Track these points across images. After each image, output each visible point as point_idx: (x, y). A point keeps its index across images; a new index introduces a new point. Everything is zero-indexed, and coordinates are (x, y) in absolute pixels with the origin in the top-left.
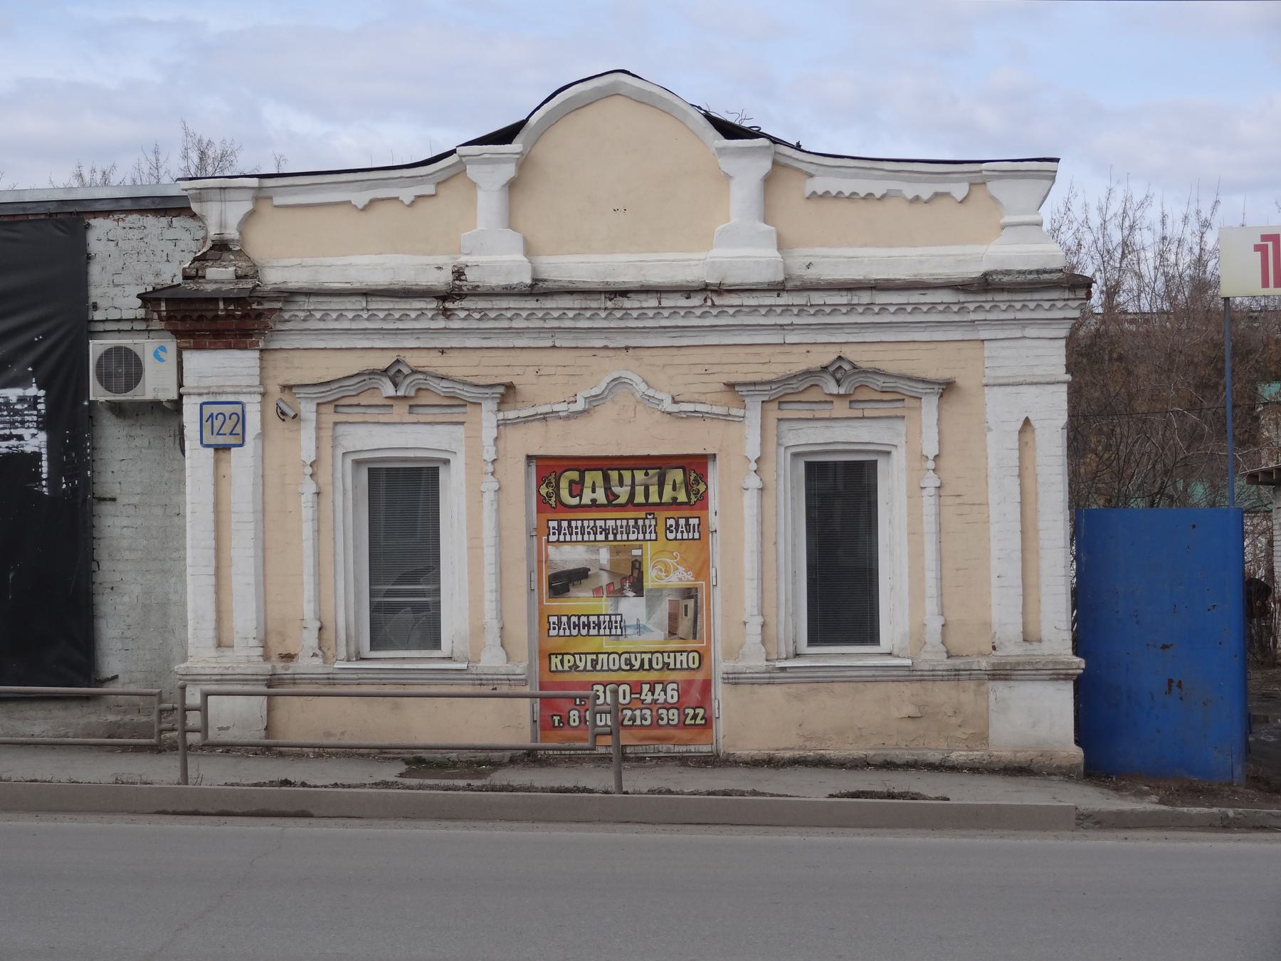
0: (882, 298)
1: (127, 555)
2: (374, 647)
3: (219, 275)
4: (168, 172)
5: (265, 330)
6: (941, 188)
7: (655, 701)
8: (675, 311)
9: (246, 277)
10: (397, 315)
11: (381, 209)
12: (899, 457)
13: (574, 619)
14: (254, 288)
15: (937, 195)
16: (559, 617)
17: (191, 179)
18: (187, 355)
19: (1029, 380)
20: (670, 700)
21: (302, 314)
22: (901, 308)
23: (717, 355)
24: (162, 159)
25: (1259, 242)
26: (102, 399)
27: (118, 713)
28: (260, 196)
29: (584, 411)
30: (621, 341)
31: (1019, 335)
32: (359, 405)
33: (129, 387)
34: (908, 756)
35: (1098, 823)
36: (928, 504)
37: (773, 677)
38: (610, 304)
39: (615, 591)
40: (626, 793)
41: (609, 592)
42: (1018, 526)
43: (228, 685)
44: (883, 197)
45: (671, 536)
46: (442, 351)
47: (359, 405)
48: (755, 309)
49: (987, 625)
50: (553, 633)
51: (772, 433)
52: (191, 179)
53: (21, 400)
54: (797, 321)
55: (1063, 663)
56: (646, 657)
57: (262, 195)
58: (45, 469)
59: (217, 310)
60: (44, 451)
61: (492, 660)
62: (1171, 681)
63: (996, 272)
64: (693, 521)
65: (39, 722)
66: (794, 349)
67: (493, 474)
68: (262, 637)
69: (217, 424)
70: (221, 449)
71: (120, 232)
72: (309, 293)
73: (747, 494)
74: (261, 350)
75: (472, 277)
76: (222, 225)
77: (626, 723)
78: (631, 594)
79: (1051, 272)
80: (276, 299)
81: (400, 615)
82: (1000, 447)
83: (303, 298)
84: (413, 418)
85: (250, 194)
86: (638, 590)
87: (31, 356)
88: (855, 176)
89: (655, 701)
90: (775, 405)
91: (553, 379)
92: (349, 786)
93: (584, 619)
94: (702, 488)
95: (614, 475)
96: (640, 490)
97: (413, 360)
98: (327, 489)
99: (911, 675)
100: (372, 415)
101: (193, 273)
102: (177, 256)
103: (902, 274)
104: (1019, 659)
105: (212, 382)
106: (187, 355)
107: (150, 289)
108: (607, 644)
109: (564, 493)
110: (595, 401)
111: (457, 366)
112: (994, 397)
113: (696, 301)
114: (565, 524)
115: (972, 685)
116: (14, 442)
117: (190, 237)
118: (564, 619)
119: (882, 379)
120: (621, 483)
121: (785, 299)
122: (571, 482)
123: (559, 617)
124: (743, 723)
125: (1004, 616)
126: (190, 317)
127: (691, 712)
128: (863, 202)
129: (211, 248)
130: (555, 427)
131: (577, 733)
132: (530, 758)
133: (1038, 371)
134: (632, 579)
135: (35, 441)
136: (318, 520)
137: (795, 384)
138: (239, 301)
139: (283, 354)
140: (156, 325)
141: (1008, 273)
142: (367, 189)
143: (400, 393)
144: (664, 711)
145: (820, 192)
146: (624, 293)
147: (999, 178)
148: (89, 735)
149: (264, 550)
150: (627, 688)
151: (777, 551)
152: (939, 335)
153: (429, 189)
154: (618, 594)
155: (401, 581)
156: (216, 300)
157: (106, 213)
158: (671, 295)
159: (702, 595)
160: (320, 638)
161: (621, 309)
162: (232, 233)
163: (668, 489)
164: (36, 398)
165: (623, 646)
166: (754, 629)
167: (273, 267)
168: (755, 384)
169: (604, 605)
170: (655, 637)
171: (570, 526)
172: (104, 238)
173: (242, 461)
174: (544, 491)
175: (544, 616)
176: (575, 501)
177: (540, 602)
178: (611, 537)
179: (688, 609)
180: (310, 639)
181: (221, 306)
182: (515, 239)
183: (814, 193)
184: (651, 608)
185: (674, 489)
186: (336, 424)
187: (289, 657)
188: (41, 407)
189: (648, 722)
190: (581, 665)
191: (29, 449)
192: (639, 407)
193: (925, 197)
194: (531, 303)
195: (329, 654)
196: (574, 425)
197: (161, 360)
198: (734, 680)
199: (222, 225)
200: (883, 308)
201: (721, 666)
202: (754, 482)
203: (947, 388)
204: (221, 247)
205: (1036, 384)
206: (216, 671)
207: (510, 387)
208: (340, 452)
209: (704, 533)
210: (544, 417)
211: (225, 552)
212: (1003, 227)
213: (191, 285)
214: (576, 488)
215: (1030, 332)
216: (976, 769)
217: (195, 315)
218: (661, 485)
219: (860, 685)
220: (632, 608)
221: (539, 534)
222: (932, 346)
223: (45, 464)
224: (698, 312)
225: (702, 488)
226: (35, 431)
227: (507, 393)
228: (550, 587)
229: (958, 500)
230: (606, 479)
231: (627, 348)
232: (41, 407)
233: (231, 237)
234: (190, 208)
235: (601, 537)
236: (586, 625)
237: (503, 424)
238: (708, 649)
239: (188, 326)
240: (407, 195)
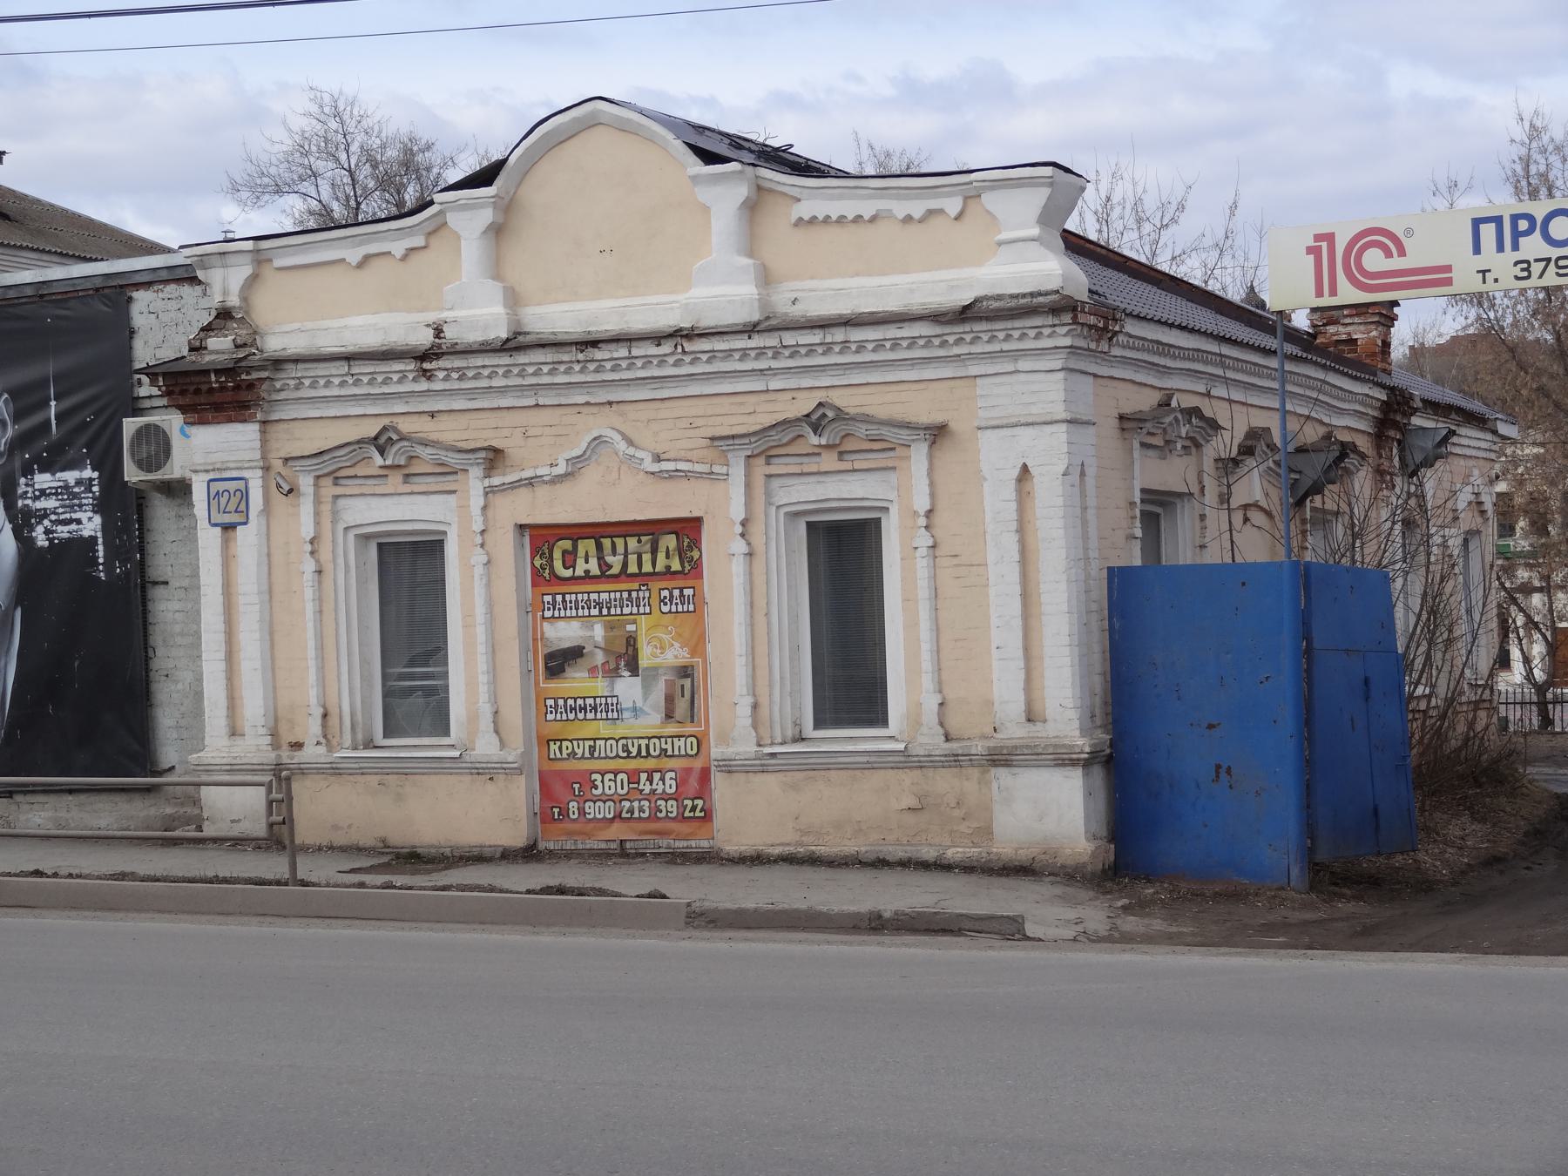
0: (857, 335)
1: (179, 640)
2: (387, 733)
5: (257, 402)
6: (934, 204)
7: (653, 792)
8: (648, 361)
9: (244, 345)
10: (380, 379)
11: (377, 264)
12: (894, 510)
13: (570, 702)
15: (931, 213)
16: (556, 700)
19: (1023, 420)
20: (668, 791)
21: (292, 383)
22: (879, 346)
23: (699, 407)
25: (1312, 243)
26: (134, 480)
27: (176, 805)
29: (567, 475)
30: (603, 396)
31: (1010, 368)
32: (356, 477)
33: (158, 468)
34: (901, 853)
35: (712, 921)
36: (922, 565)
37: (764, 765)
38: (581, 356)
39: (610, 671)
40: (304, 883)
41: (604, 672)
42: (1018, 589)
43: (236, 774)
44: (873, 219)
45: (665, 609)
46: (432, 415)
47: (356, 477)
48: (729, 353)
49: (989, 703)
50: (550, 717)
51: (759, 491)
53: (79, 482)
54: (775, 364)
55: (1064, 746)
56: (643, 742)
58: (101, 554)
60: (99, 534)
61: (486, 747)
62: (1218, 767)
63: (987, 298)
64: (688, 592)
65: (105, 814)
66: (779, 396)
67: (482, 545)
68: (272, 723)
69: (223, 501)
70: (228, 528)
71: (160, 304)
72: (297, 360)
73: (735, 559)
75: (450, 333)
76: (225, 292)
77: (624, 815)
78: (627, 673)
79: (1047, 294)
80: (262, 368)
81: (411, 700)
82: (998, 500)
84: (408, 488)
85: (248, 258)
86: (634, 669)
87: (84, 439)
88: (841, 198)
89: (653, 792)
90: (761, 460)
91: (540, 442)
92: (79, 876)
93: (580, 702)
94: (696, 554)
95: (607, 542)
96: (633, 558)
97: (405, 426)
98: (328, 568)
99: (906, 761)
100: (370, 486)
101: (197, 344)
103: (892, 305)
104: (1018, 742)
105: (217, 458)
108: (604, 729)
109: (558, 564)
110: (577, 465)
111: (448, 431)
112: (988, 440)
113: (666, 348)
114: (559, 598)
115: (975, 773)
116: (74, 527)
118: (561, 702)
119: (864, 426)
120: (614, 553)
121: (757, 341)
122: (564, 553)
123: (556, 700)
124: (747, 814)
125: (1006, 691)
127: (689, 803)
128: (853, 226)
130: (542, 491)
131: (576, 826)
132: (530, 854)
133: (1034, 410)
134: (627, 658)
135: (91, 525)
136: (320, 600)
137: (776, 437)
139: (282, 426)
141: (999, 297)
142: (360, 244)
143: (389, 462)
144: (662, 803)
145: (806, 218)
146: (594, 344)
147: (992, 188)
148: (148, 828)
149: (271, 634)
150: (624, 776)
151: (769, 624)
152: (929, 373)
153: (419, 241)
154: (612, 673)
155: (411, 663)
156: (206, 372)
157: (147, 285)
158: (641, 344)
159: (699, 674)
160: (324, 726)
161: (593, 361)
162: (234, 301)
163: (661, 556)
164: (91, 480)
165: (620, 731)
166: (744, 710)
168: (733, 437)
169: (600, 686)
170: (652, 721)
171: (564, 600)
172: (145, 310)
173: (247, 537)
174: (538, 563)
175: (541, 699)
176: (568, 573)
177: (537, 683)
178: (605, 611)
179: (685, 690)
180: (315, 727)
181: (213, 378)
182: (494, 290)
183: (801, 219)
184: (647, 689)
185: (668, 557)
186: (336, 497)
187: (297, 746)
188: (95, 489)
189: (646, 815)
190: (579, 752)
191: (86, 533)
192: (624, 468)
193: (917, 215)
194: (505, 360)
195: (334, 742)
196: (562, 489)
198: (728, 768)
199: (225, 292)
200: (861, 347)
201: (716, 751)
202: (740, 546)
203: (937, 433)
204: (224, 314)
205: (1032, 424)
206: (224, 761)
207: (497, 452)
208: (341, 526)
209: (698, 601)
210: (530, 482)
211: (254, 634)
212: (1000, 244)
214: (569, 558)
215: (1024, 365)
216: (968, 868)
217: (192, 388)
218: (654, 552)
219: (858, 773)
220: (628, 689)
221: (535, 611)
222: (922, 386)
223: (101, 548)
224: (671, 360)
225: (696, 554)
226: (90, 514)
227: (494, 458)
228: (547, 668)
229: (955, 561)
230: (599, 547)
231: (610, 403)
232: (95, 489)
235: (595, 612)
236: (582, 708)
237: (489, 492)
238: (706, 733)
239: (187, 400)
240: (398, 248)
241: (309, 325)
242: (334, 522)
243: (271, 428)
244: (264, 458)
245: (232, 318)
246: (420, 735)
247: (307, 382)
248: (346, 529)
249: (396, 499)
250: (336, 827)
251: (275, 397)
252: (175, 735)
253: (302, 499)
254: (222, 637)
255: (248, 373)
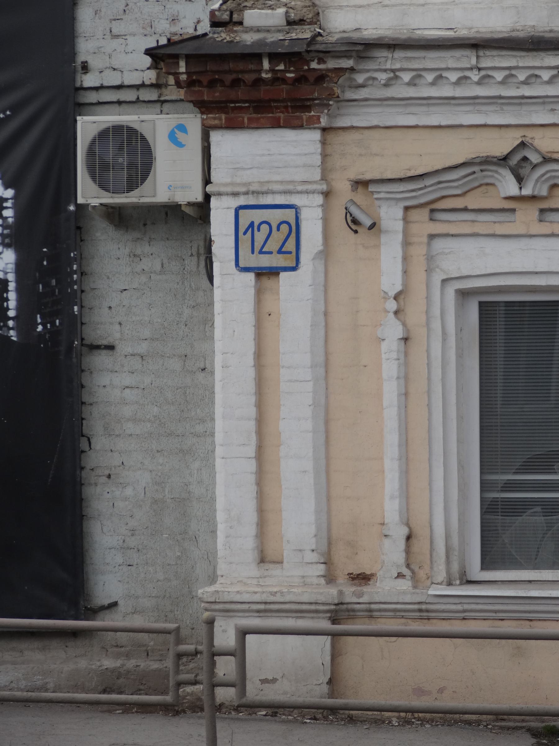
1: (130, 428)
2: (486, 565)
5: (329, 99)
9: (301, 22)
21: (383, 77)
26: (95, 202)
27: (117, 656)
32: (465, 210)
43: (274, 617)
47: (465, 210)
58: (12, 303)
60: (11, 277)
69: (260, 237)
70: (265, 274)
80: (346, 55)
84: (545, 228)
101: (226, 17)
136: (405, 378)
148: (77, 688)
149: (327, 422)
155: (526, 468)
156: (257, 57)
160: (408, 551)
173: (295, 291)
180: (393, 553)
181: (266, 65)
186: (432, 237)
187: (363, 578)
195: (422, 574)
206: (257, 598)
217: (228, 78)
223: (12, 296)
239: (218, 94)
242: (429, 271)
243: (335, 139)
244: (324, 178)
246: (536, 567)
247: (406, 77)
248: (444, 281)
249: (524, 242)
250: (419, 691)
251: (350, 95)
252: (119, 559)
253: (384, 238)
254: (252, 425)
255: (321, 61)
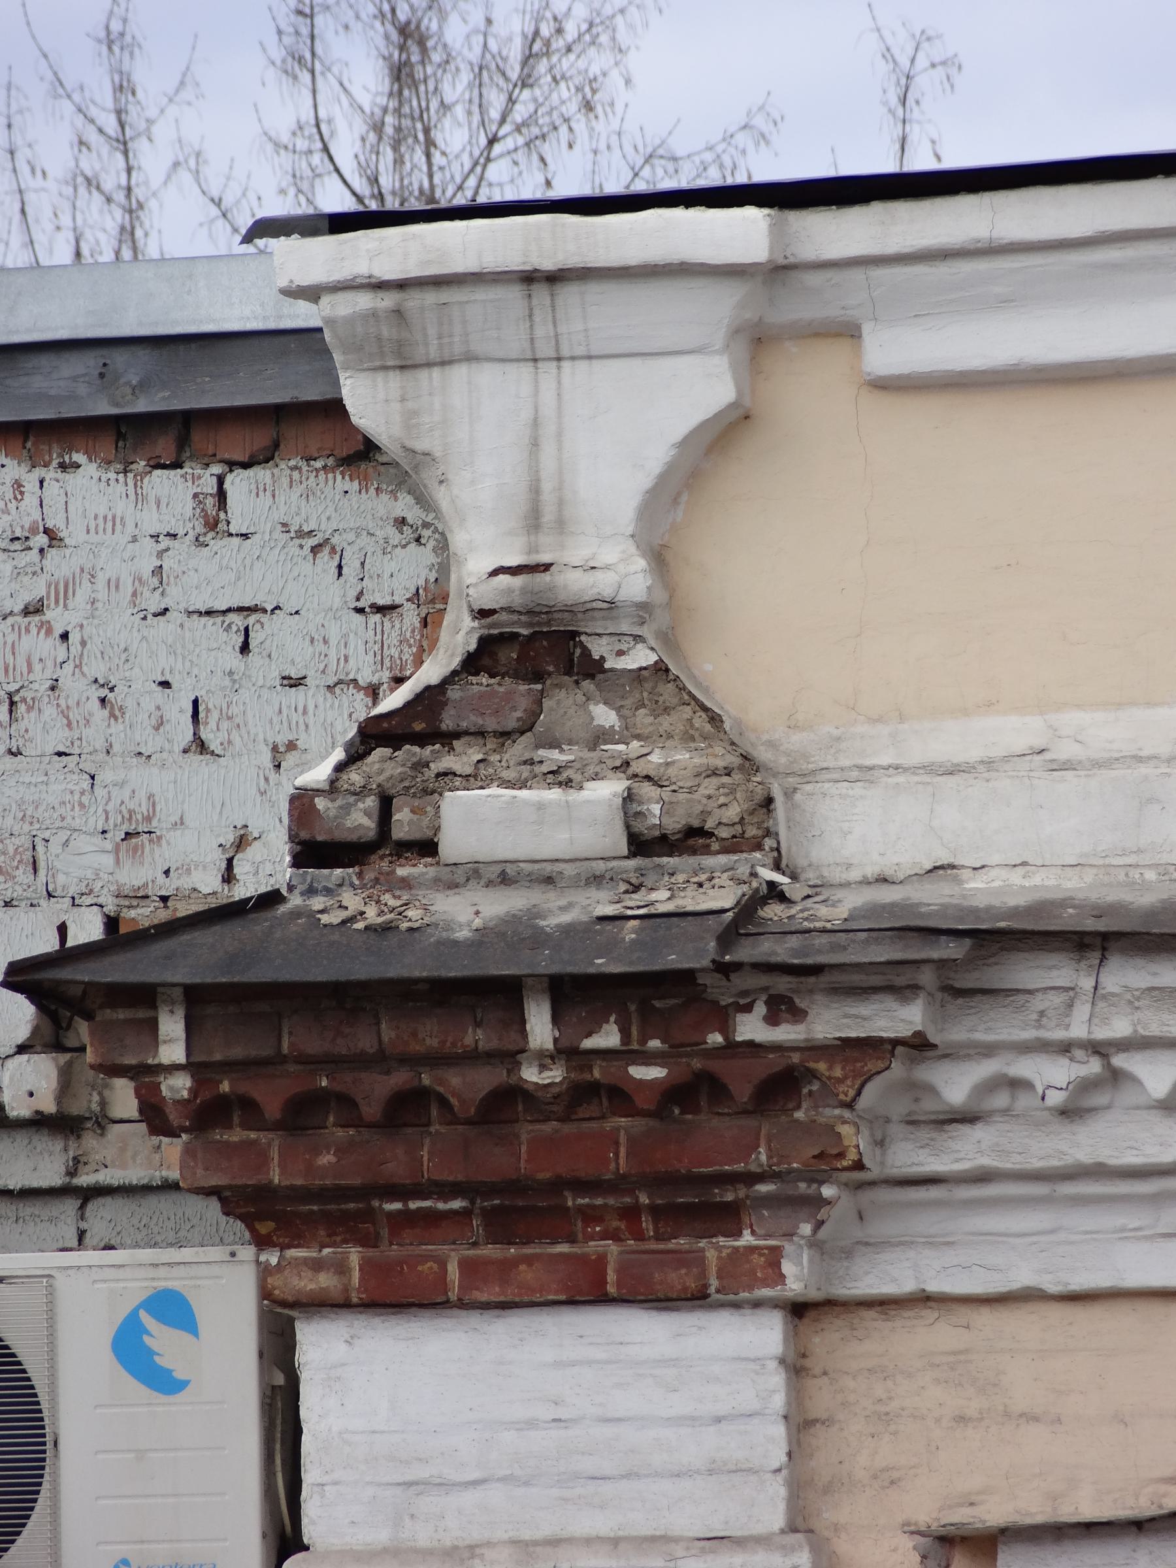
3: (526, 835)
4: (189, 162)
9: (693, 839)
14: (748, 909)
17: (340, 223)
18: (326, 1349)
21: (1055, 1075)
24: (152, 79)
28: (777, 318)
52: (340, 223)
57: (796, 308)
59: (512, 1057)
74: (798, 1310)
80: (892, 982)
83: (1056, 972)
85: (720, 306)
101: (360, 820)
102: (260, 713)
106: (326, 1349)
107: (87, 929)
117: (338, 594)
126: (346, 1102)
129: (472, 664)
138: (657, 996)
140: (129, 1154)
156: (501, 995)
162: (602, 563)
167: (866, 773)
181: (540, 1027)
197: (164, 1382)
204: (537, 649)
213: (348, 900)
217: (376, 1089)
233: (602, 585)
234: (334, 409)
239: (328, 1158)
241: (1103, 731)
245: (591, 669)
251: (911, 1155)
255: (781, 1009)
